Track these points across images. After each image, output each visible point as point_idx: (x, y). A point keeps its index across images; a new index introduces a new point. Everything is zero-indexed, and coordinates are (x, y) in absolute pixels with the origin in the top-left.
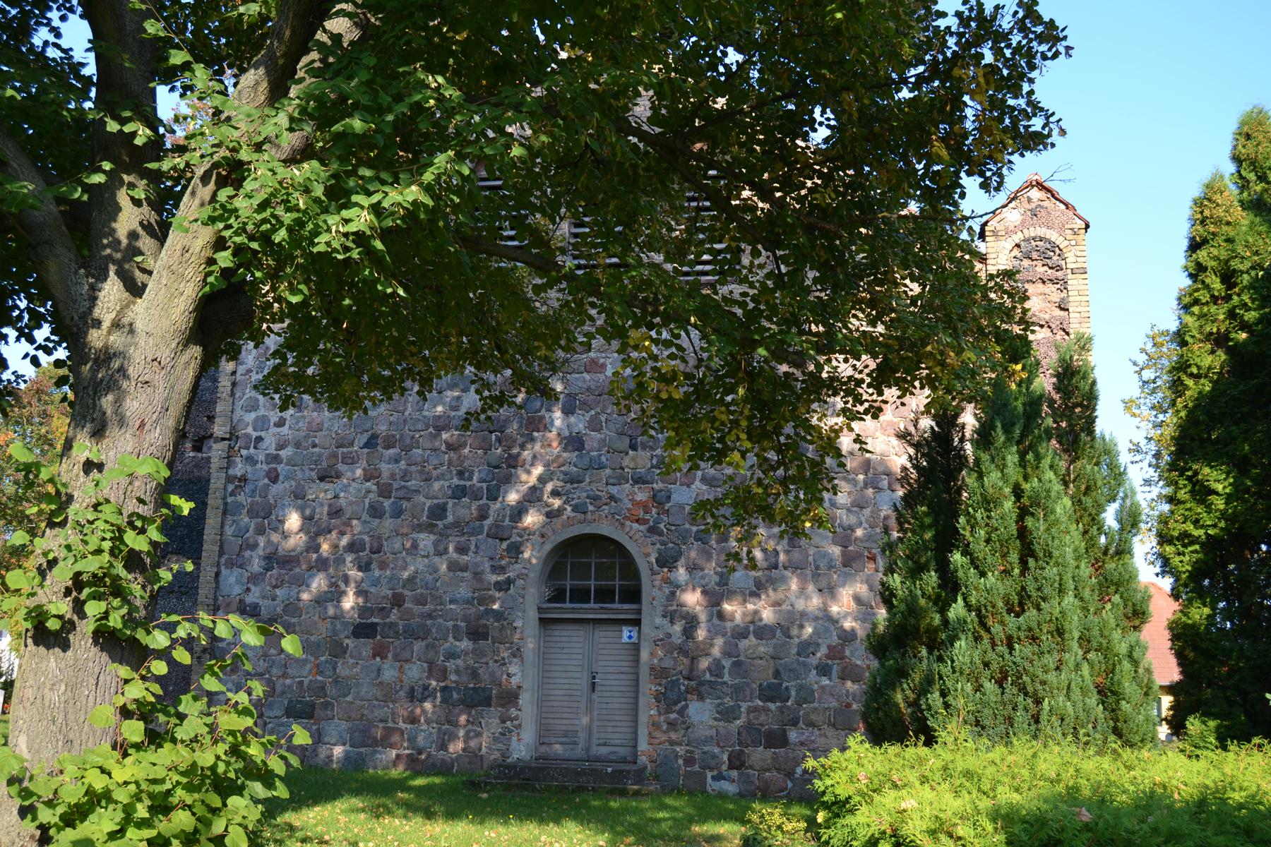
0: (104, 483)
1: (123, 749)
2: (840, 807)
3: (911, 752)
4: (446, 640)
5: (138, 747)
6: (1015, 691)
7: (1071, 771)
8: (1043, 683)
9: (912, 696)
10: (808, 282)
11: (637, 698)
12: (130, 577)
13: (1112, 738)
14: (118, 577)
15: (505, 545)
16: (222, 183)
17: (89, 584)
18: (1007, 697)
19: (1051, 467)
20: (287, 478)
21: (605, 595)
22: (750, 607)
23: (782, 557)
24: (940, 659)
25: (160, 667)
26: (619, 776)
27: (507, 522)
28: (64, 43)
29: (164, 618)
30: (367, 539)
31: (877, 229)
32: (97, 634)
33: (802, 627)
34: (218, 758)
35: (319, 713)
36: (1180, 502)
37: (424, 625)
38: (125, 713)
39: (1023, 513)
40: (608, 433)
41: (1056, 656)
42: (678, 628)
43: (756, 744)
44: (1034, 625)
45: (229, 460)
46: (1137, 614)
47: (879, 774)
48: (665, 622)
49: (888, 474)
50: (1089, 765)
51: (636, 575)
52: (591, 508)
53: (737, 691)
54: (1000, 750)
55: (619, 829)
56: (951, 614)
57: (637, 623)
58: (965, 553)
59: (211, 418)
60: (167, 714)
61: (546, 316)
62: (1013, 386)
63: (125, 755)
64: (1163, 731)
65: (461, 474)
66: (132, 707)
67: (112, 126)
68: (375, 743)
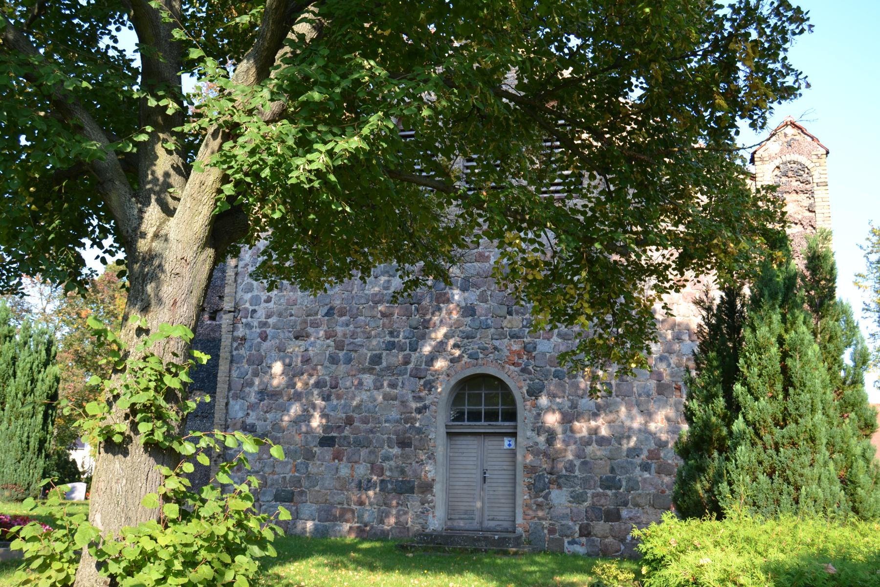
0: (150, 343)
1: (165, 523)
2: (657, 563)
4: (383, 448)
5: (174, 521)
6: (781, 481)
7: (822, 537)
8: (801, 475)
10: (629, 197)
11: (515, 487)
12: (168, 406)
13: (851, 514)
14: (160, 406)
15: (422, 382)
16: (226, 138)
17: (141, 411)
18: (775, 485)
19: (804, 323)
20: (273, 338)
21: (491, 416)
24: (727, 459)
25: (189, 468)
26: (503, 541)
27: (423, 366)
28: (120, 46)
29: (191, 434)
30: (327, 378)
32: (147, 445)
34: (228, 529)
35: (296, 498)
37: (367, 438)
38: (166, 498)
39: (785, 355)
40: (492, 304)
42: (542, 439)
43: (598, 519)
44: (794, 434)
45: (234, 325)
48: (534, 434)
51: (513, 402)
52: (481, 356)
53: (585, 482)
54: (771, 523)
55: (504, 578)
56: (735, 428)
57: (514, 435)
58: (743, 385)
59: (221, 298)
60: (194, 499)
63: (166, 527)
65: (391, 333)
66: (171, 494)
67: (152, 103)
68: (335, 519)
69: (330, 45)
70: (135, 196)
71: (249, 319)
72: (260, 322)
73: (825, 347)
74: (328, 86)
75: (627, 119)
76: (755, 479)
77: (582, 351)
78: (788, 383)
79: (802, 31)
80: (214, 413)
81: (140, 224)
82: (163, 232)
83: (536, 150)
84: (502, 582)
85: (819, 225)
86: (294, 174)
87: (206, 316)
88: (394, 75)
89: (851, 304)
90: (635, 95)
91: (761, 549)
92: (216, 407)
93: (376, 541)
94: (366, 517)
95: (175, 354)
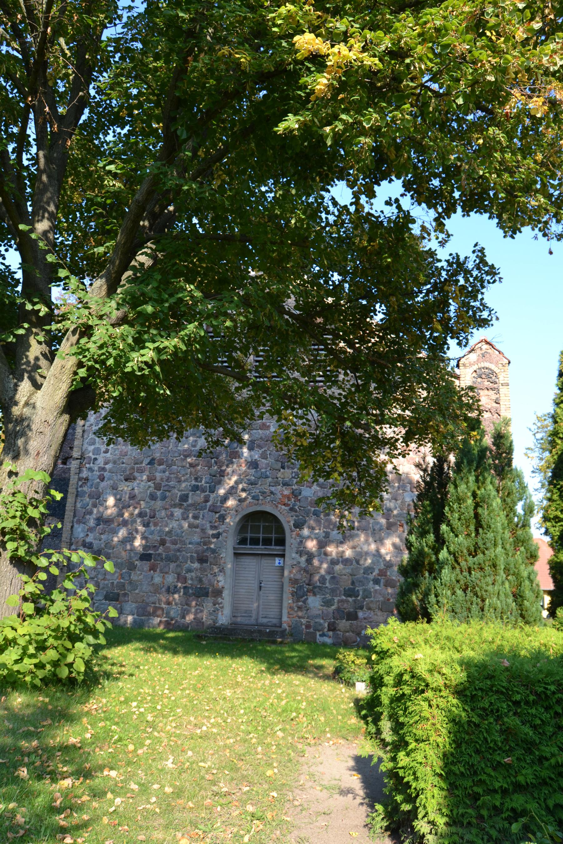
0: (18, 483)
1: (23, 617)
2: (384, 654)
3: (420, 627)
4: (186, 563)
5: (30, 616)
6: (472, 595)
7: (500, 637)
8: (486, 591)
9: (421, 597)
10: (371, 389)
11: (282, 594)
12: (30, 530)
13: (520, 619)
14: (23, 530)
15: (217, 515)
16: (82, 335)
17: (9, 533)
18: (468, 598)
19: (491, 483)
20: (109, 479)
21: (267, 542)
22: (340, 549)
23: (356, 524)
24: (435, 578)
25: (43, 576)
26: (272, 633)
27: (219, 504)
28: (7, 262)
29: (46, 551)
30: (148, 510)
31: (406, 364)
32: (12, 559)
33: (366, 559)
34: (71, 623)
35: (121, 598)
36: (554, 501)
37: (175, 555)
38: (25, 599)
39: (477, 505)
40: (271, 460)
41: (492, 578)
42: (303, 559)
43: (342, 618)
44: (482, 562)
45: (80, 469)
46: (532, 557)
47: (403, 637)
48: (297, 556)
49: (411, 482)
50: (508, 634)
51: (283, 532)
52: (261, 498)
53: (333, 591)
54: (464, 625)
55: (272, 661)
56: (441, 556)
57: (283, 556)
58: (448, 525)
59: (71, 448)
60: (46, 600)
61: (239, 402)
62: (472, 442)
63: (24, 620)
64: (545, 613)
65: (196, 479)
66: (28, 596)
67: (29, 307)
68: (149, 615)
69: (163, 272)
70: (12, 373)
73: (505, 500)
74: (160, 301)
75: (372, 334)
76: (454, 593)
77: (334, 497)
78: (479, 525)
79: (494, 281)
81: (15, 395)
82: (32, 401)
83: (306, 352)
84: (271, 664)
85: (503, 413)
86: (130, 364)
87: (60, 461)
88: (207, 296)
89: (523, 471)
90: (378, 318)
91: (457, 645)
93: (180, 631)
94: (172, 613)
95: (36, 492)
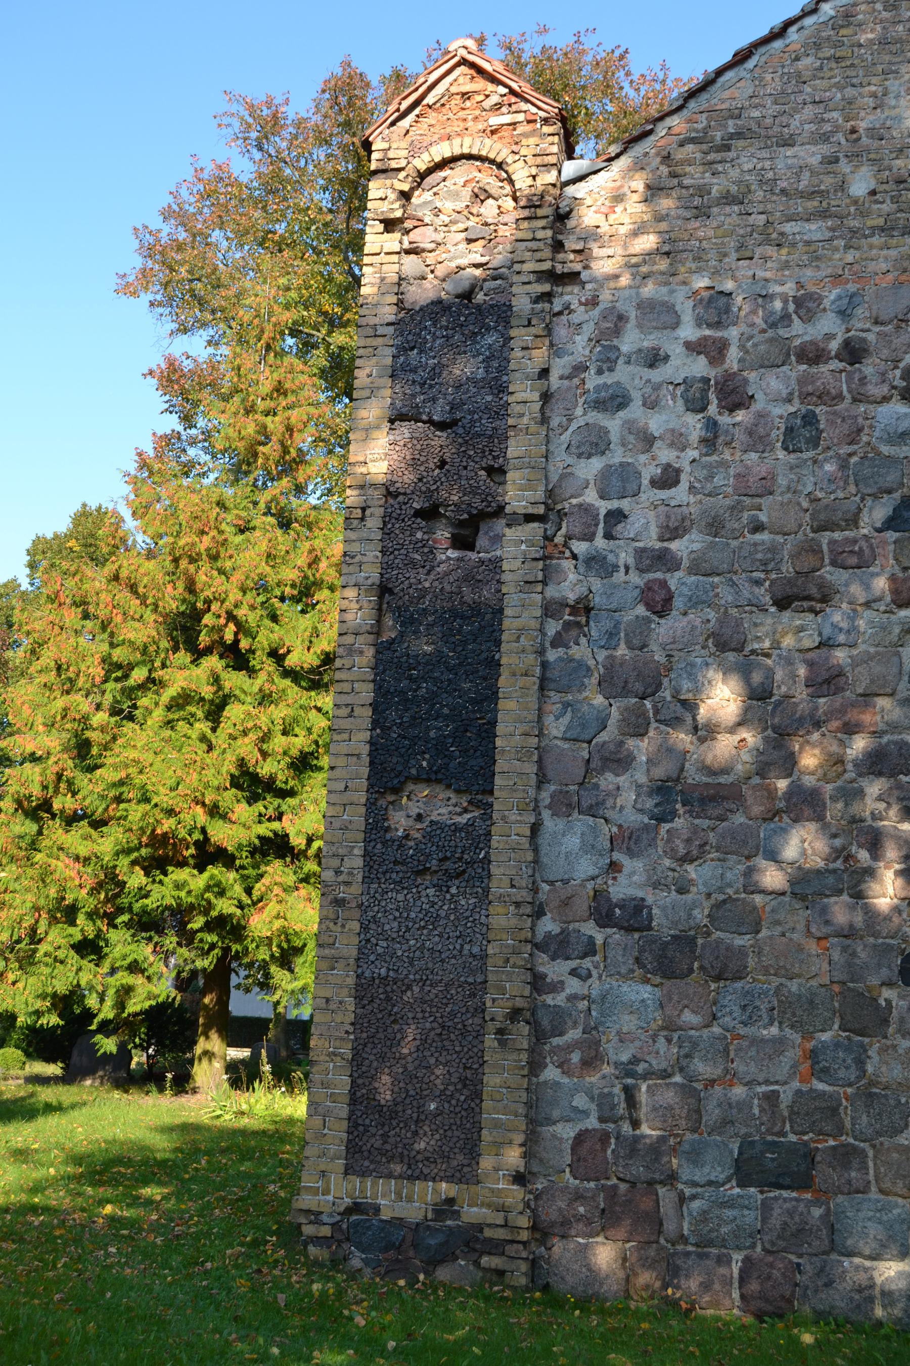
20: (695, 603)
35: (824, 1174)
59: (497, 472)
71: (600, 542)
72: (640, 553)
80: (487, 860)
92: (495, 841)
